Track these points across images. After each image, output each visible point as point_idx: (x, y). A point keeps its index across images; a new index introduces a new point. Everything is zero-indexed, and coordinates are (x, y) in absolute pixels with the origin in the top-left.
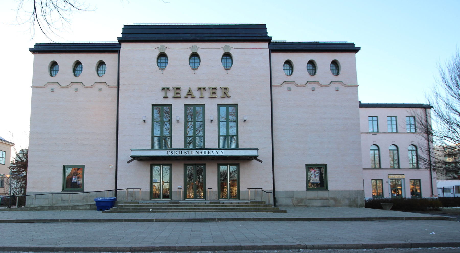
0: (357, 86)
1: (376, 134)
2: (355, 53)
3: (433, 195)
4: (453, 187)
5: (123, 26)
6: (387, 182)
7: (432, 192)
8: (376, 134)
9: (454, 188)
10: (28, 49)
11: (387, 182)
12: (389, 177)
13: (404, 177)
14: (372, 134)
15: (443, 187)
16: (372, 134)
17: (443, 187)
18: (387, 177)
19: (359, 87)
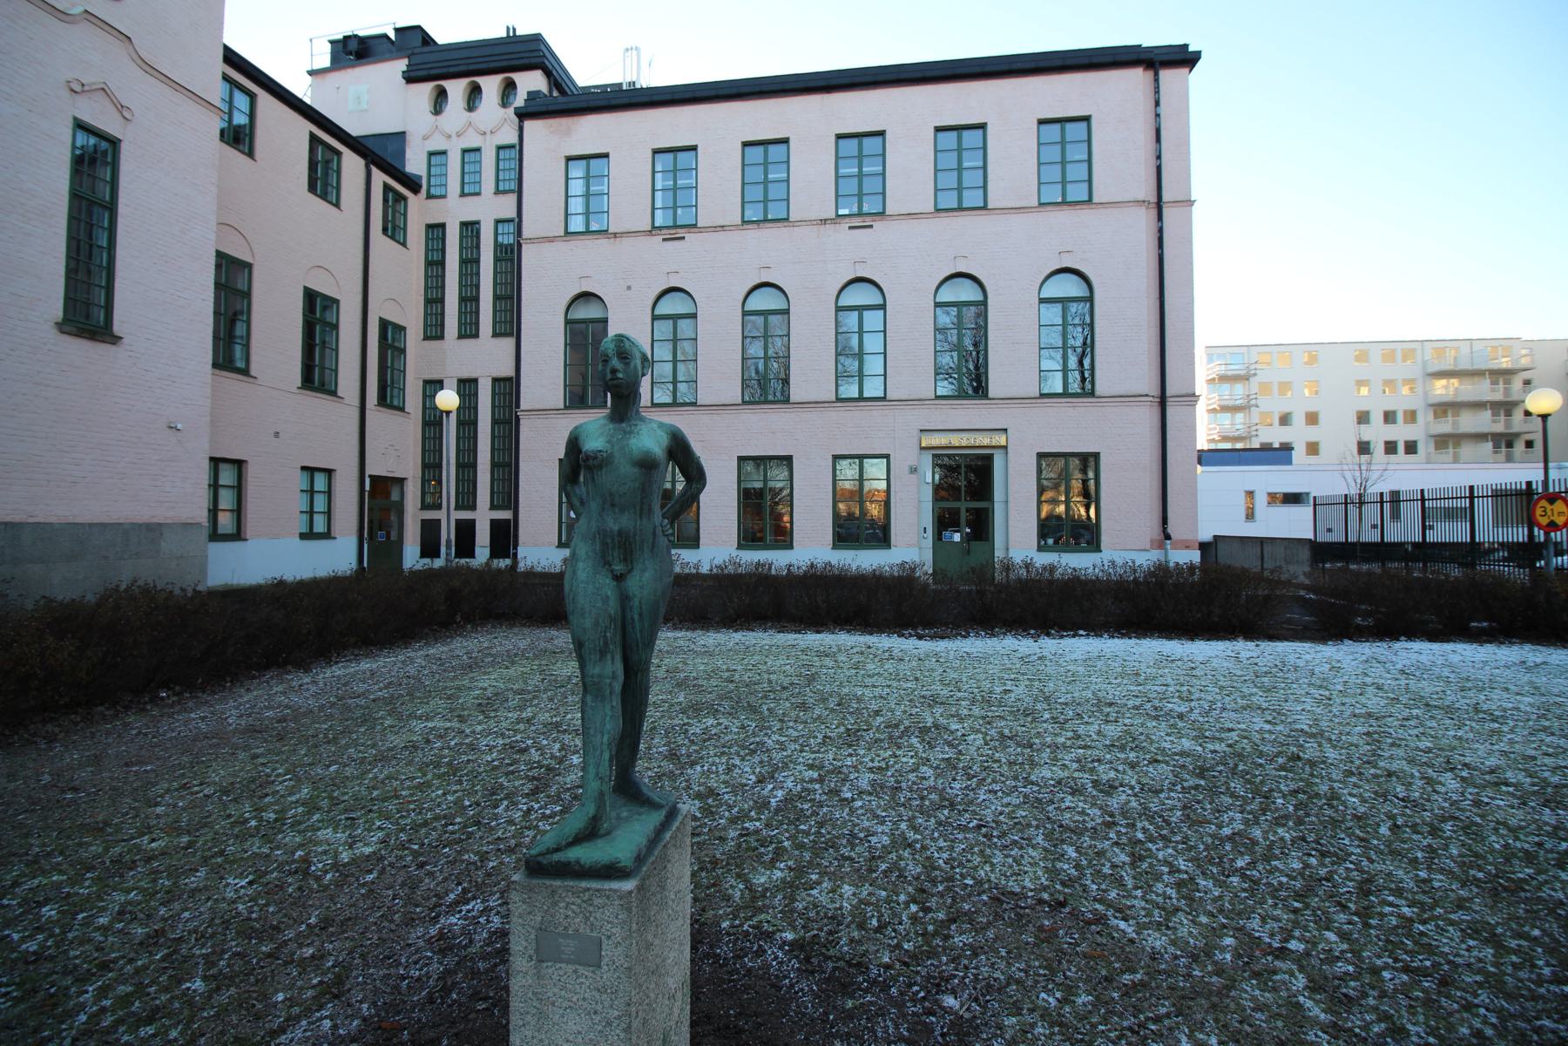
0: (1190, 203)
1: (871, 226)
2: (1187, 70)
3: (1168, 537)
4: (1382, 494)
5: (329, 45)
6: (914, 470)
7: (1165, 520)
8: (871, 226)
9: (1382, 502)
10: (1287, 410)
11: (914, 470)
12: (923, 445)
13: (1001, 440)
14: (850, 228)
15: (1471, 488)
16: (850, 228)
17: (1471, 488)
18: (916, 440)
19: (1195, 208)
